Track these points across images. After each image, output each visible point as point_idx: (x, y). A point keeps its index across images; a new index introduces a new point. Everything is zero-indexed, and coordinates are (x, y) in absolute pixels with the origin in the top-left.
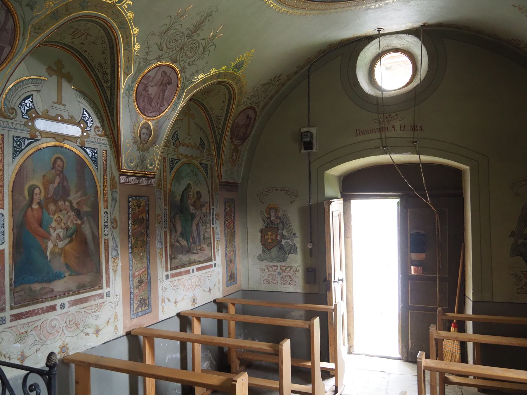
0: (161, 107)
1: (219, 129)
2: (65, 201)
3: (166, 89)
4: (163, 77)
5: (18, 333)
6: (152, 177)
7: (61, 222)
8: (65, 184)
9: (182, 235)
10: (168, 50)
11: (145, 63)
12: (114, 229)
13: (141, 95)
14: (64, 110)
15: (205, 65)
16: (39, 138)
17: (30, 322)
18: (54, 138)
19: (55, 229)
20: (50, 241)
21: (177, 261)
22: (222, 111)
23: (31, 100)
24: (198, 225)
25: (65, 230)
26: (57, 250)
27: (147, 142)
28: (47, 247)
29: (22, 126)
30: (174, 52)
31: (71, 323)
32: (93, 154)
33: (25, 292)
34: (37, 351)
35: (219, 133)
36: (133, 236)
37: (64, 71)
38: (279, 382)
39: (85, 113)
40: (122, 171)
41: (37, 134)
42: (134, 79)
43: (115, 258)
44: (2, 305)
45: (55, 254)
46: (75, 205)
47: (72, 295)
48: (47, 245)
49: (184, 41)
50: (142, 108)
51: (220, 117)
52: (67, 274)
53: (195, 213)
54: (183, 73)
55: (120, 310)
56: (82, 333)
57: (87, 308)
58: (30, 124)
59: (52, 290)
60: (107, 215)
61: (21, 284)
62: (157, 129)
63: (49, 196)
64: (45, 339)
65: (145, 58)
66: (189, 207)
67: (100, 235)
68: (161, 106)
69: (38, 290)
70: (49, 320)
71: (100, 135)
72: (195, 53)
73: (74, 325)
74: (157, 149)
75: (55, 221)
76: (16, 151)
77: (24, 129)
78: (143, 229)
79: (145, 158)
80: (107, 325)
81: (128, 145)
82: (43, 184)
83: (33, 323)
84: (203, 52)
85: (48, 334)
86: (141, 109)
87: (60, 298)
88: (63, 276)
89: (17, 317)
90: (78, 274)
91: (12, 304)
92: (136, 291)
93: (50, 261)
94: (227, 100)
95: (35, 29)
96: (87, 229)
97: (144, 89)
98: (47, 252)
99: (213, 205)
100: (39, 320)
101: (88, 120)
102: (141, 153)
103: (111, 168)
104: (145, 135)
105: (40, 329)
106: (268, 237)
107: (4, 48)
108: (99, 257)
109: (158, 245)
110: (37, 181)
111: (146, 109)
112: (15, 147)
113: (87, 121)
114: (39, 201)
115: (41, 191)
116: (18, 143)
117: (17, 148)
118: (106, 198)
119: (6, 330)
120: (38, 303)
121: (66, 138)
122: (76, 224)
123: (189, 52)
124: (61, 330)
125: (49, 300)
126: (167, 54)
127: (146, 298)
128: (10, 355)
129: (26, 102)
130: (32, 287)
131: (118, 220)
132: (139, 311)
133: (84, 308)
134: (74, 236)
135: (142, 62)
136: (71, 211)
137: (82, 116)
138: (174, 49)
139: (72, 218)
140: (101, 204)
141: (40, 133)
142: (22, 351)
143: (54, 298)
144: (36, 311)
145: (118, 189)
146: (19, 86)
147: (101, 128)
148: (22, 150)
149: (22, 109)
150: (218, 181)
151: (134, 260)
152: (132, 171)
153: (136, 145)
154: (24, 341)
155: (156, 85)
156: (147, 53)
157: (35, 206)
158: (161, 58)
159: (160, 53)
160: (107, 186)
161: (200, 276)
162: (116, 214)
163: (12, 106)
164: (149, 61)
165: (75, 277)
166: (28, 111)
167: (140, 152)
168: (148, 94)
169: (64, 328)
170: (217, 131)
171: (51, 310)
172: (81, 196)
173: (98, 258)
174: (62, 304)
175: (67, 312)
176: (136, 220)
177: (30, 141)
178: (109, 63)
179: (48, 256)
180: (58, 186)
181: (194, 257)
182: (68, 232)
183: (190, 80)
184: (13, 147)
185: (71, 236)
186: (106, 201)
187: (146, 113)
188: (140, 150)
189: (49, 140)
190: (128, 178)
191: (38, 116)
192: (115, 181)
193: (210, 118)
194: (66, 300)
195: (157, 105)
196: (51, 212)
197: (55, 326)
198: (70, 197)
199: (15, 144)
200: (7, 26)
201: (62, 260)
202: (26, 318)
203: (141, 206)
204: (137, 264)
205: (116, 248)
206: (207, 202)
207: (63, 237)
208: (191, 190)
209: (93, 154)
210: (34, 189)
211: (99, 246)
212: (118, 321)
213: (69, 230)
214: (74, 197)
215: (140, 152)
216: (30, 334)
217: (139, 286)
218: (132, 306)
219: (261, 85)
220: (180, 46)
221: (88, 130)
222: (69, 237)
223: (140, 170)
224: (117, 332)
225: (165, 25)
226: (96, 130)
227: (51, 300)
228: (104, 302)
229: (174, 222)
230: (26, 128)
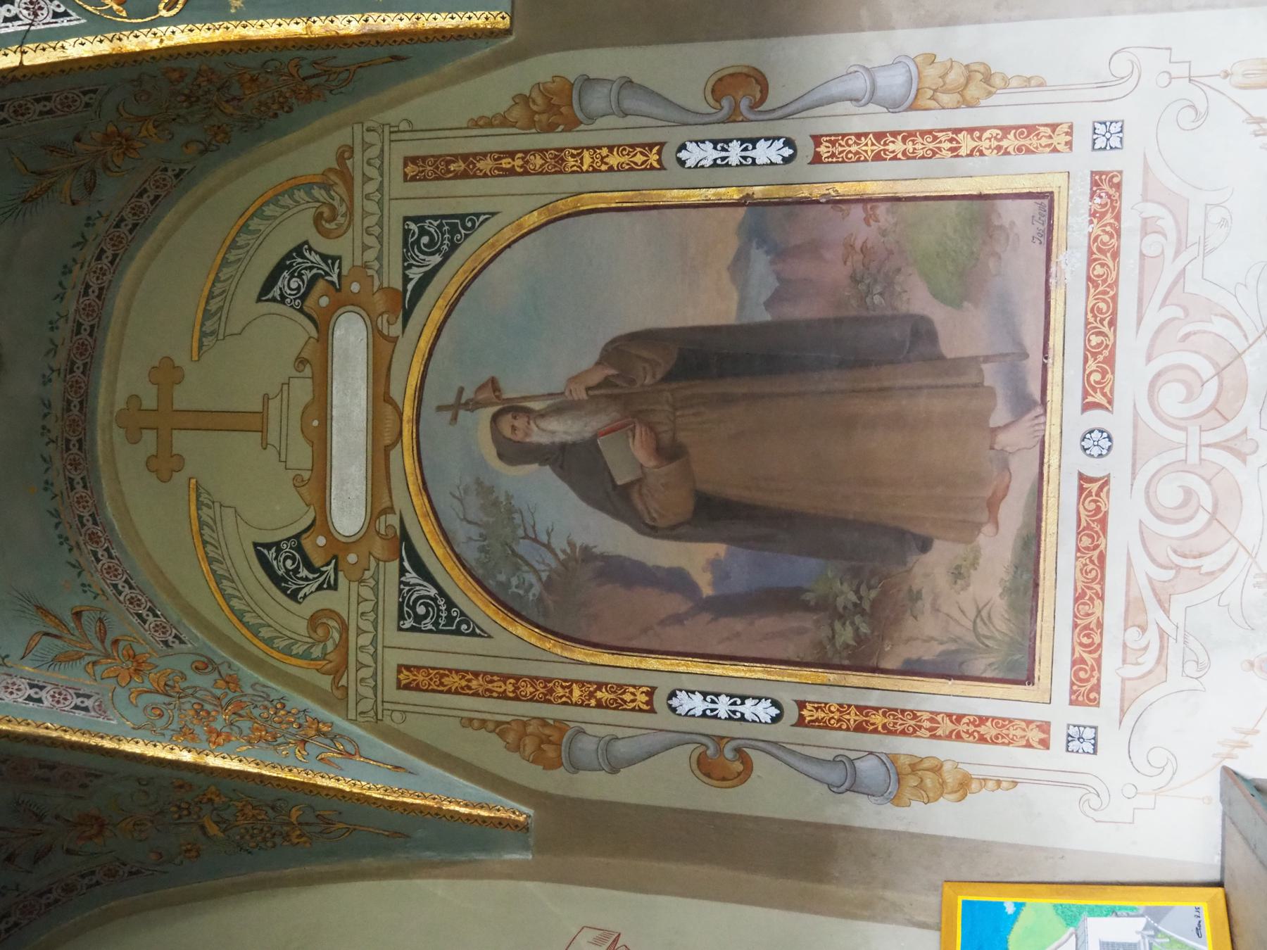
12: (763, 100)
14: (1117, 82)
16: (393, 520)
18: (387, 449)
23: (273, 550)
32: (425, 240)
38: (619, 483)
39: (276, 292)
101: (300, 276)
103: (490, 124)
116: (421, 610)
117: (439, 616)
129: (281, 572)
148: (442, 593)
191: (321, 522)
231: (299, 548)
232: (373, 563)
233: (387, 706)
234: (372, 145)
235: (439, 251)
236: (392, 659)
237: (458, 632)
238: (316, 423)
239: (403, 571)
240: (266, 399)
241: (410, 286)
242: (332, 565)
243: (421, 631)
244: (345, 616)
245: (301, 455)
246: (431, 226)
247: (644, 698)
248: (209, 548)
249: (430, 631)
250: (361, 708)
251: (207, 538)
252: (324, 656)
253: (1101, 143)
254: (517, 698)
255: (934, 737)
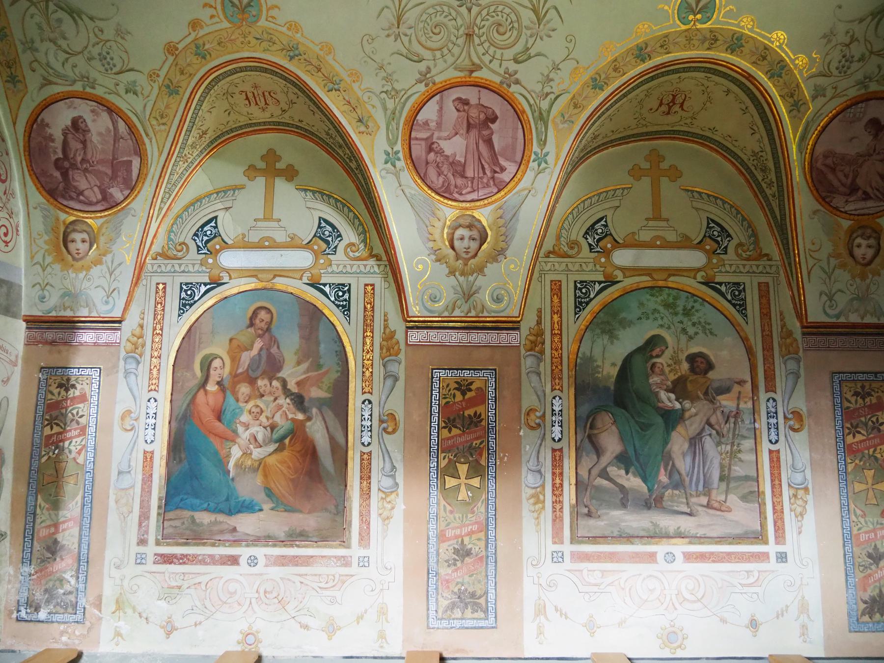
0: (496, 175)
1: (770, 185)
2: (271, 380)
3: (492, 134)
4: (464, 111)
5: (166, 586)
6: (513, 326)
7: (261, 415)
8: (274, 350)
9: (623, 460)
10: (438, 54)
11: (397, 100)
12: (389, 433)
13: (427, 163)
15: (571, 46)
16: (226, 279)
17: (187, 573)
18: (649, 275)
19: (247, 426)
20: (237, 445)
21: (602, 523)
22: (757, 136)
24: (695, 441)
25: (268, 428)
26: (249, 463)
27: (476, 255)
28: (229, 455)
29: (197, 267)
30: (456, 51)
31: (268, 596)
32: (340, 294)
33: (183, 523)
34: (196, 625)
35: (774, 196)
36: (442, 452)
37: (280, 165)
39: (323, 224)
40: (408, 319)
41: (221, 275)
42: (391, 137)
43: (386, 494)
44: (143, 535)
45: (245, 468)
46: (292, 386)
47: (274, 546)
48: (230, 451)
49: (463, 18)
50: (443, 186)
51: (761, 154)
52: (266, 507)
53: (683, 410)
54: (512, 85)
55: (395, 600)
56: (293, 620)
57: (308, 577)
58: (210, 261)
59: (234, 530)
60: (370, 406)
61: (177, 508)
62: (501, 222)
63: (240, 370)
64: (214, 610)
65: (390, 88)
66: (656, 394)
67: (350, 444)
68: (495, 172)
69: (206, 523)
70: (223, 581)
71: (359, 259)
72: (515, 33)
73: (276, 601)
74: (512, 266)
75: (248, 414)
76: (184, 305)
77: (200, 270)
78: (477, 439)
79: (474, 288)
80: (358, 623)
81: (420, 266)
82: (228, 353)
83: (193, 576)
84: (538, 20)
85: (220, 603)
86: (439, 191)
87: (247, 546)
88: (257, 508)
89: (167, 559)
90: (290, 509)
91: (160, 537)
92: (445, 571)
93: (233, 479)
94: (748, 102)
95: (157, 120)
96: (317, 431)
97: (430, 149)
98: (228, 463)
99: (771, 387)
100: (204, 574)
101: (329, 236)
102: (461, 279)
104: (466, 241)
105: (204, 588)
106: (463, 476)
107: (131, 162)
108: (346, 486)
109: (530, 479)
110: (219, 348)
111: (452, 187)
112: (183, 299)
113: (328, 239)
114: (220, 379)
115: (224, 363)
116: (189, 293)
117: (186, 300)
118: (367, 374)
119: (146, 574)
120: (204, 544)
121: (278, 273)
122: (293, 420)
123: (496, 34)
124: (248, 602)
125: (227, 545)
126: (440, 62)
127: (478, 593)
128: (149, 615)
129: (205, 229)
130: (196, 517)
131: (400, 416)
132: (453, 616)
133: (300, 575)
134: (287, 441)
135: (387, 99)
136: (283, 397)
137: (317, 231)
138: (450, 45)
139: (283, 409)
140: (355, 385)
141: (228, 273)
142: (169, 616)
143: (236, 542)
144: (200, 558)
145: (402, 356)
146: (599, 199)
147: (362, 246)
149: (198, 241)
150: (795, 326)
151: (443, 502)
152: (439, 317)
153: (488, 264)
154: (174, 601)
155: (456, 134)
156: (388, 79)
157: (212, 387)
158: (428, 76)
159: (422, 66)
160: (372, 351)
161: (702, 576)
162: (396, 404)
163: (181, 240)
164: (403, 92)
165: (285, 514)
166: (207, 242)
167: (459, 277)
168: (447, 156)
169: (253, 601)
170: (768, 192)
171: (229, 563)
172: (308, 371)
173: (342, 487)
174: (252, 558)
175: (261, 575)
176: (454, 420)
177: (208, 287)
178: (331, 127)
179: (231, 470)
180: (259, 354)
181: (668, 522)
182: (274, 432)
183: (547, 94)
184: (180, 299)
185: (281, 440)
186: (367, 381)
187: (456, 196)
188: (457, 274)
189: (243, 280)
190: (432, 333)
192: (394, 341)
193: (742, 162)
194: (261, 552)
195: (484, 173)
196: (241, 398)
197: (235, 592)
198: (282, 372)
199: (183, 295)
200: (120, 131)
201: (259, 480)
202: (181, 564)
203: (470, 390)
204: (451, 512)
205: (393, 473)
206: (741, 383)
207: (264, 441)
208: (663, 352)
209: (737, 293)
210: (212, 360)
211: (346, 464)
212: (387, 622)
213: (276, 429)
214: (292, 373)
215: (459, 277)
216: (185, 592)
217: (455, 560)
218: (432, 601)
219: (861, 20)
220: (461, 32)
221: (329, 254)
222: (276, 442)
223: (462, 315)
224: (385, 645)
225: (383, 9)
226: (349, 250)
227: (230, 546)
228: (352, 576)
229: (591, 428)
230: (204, 268)
231: (215, 237)
232: (208, 270)
233: (543, 276)
234: (744, 268)
235: (336, 300)
236: (168, 280)
237: (576, 307)
238: (658, 243)
239: (600, 283)
240: (667, 220)
241: (718, 286)
242: (207, 252)
243: (181, 292)
244: (579, 256)
245: (254, 237)
246: (346, 296)
247: (367, 391)
248: (215, 195)
249: (575, 295)
250: (584, 265)
251: (609, 193)
252: (169, 248)
253: (361, 564)
254: (552, 334)
255: (553, 503)
